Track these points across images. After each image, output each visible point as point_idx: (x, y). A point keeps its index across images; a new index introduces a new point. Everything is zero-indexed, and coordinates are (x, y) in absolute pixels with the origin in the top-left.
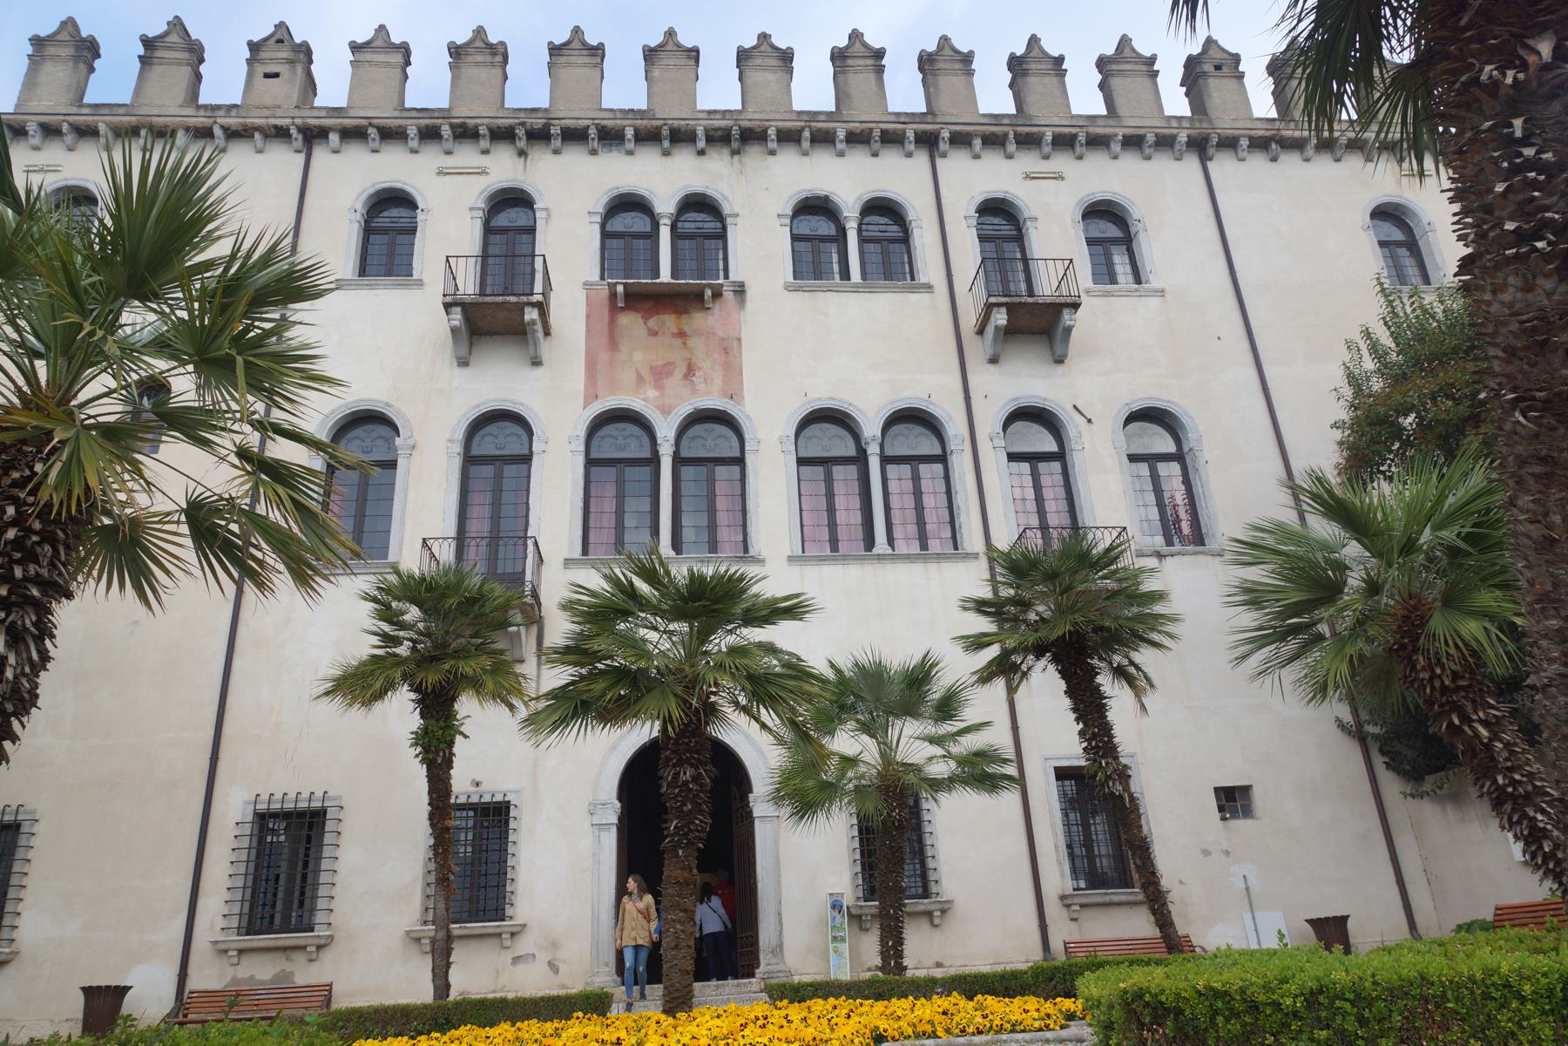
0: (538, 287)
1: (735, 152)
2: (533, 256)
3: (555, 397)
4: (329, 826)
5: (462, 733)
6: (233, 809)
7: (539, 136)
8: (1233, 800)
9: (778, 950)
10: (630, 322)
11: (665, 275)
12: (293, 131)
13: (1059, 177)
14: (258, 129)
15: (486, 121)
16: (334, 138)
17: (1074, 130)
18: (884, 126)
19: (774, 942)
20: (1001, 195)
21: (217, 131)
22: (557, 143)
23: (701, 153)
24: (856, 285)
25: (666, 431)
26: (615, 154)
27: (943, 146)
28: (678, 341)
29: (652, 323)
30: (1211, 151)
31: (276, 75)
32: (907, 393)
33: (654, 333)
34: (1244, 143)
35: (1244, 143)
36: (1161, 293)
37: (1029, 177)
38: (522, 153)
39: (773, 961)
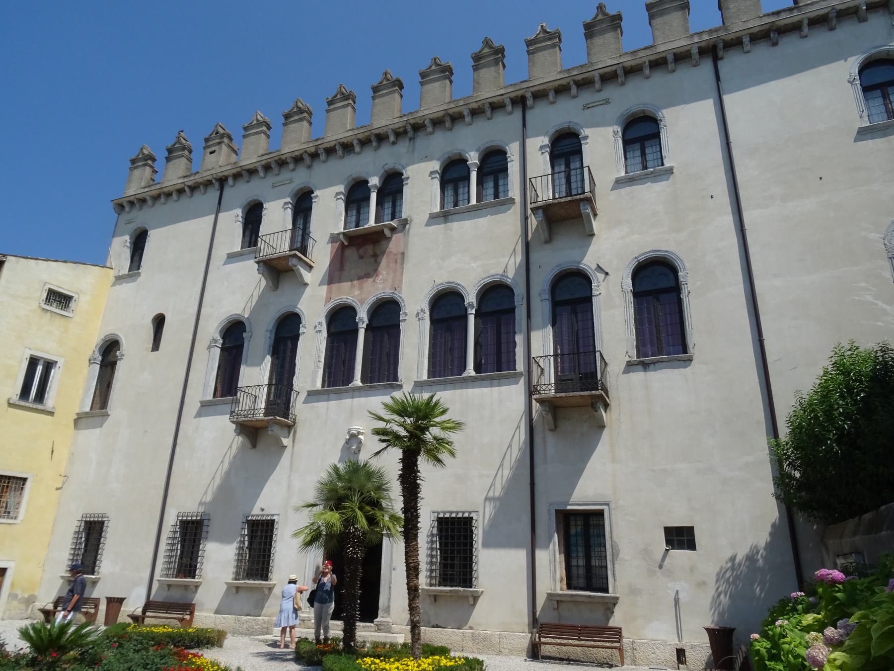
0: (587, 189)
1: (411, 139)
2: (582, 167)
3: (314, 304)
4: (204, 529)
5: (643, 154)
6: (171, 519)
7: (456, 118)
8: (680, 537)
9: (388, 610)
10: (351, 253)
11: (372, 222)
12: (214, 181)
13: (607, 102)
14: (201, 183)
15: (745, 32)
16: (230, 181)
17: (614, 68)
18: (489, 100)
19: (386, 604)
20: (566, 125)
21: (187, 189)
22: (671, 66)
23: (394, 143)
24: (476, 208)
25: (471, 298)
26: (352, 155)
27: (530, 102)
28: (372, 260)
29: (361, 251)
30: (720, 54)
31: (214, 152)
32: (492, 272)
33: (361, 257)
34: (746, 40)
35: (746, 40)
36: (670, 171)
37: (586, 107)
38: (309, 167)
39: (385, 615)
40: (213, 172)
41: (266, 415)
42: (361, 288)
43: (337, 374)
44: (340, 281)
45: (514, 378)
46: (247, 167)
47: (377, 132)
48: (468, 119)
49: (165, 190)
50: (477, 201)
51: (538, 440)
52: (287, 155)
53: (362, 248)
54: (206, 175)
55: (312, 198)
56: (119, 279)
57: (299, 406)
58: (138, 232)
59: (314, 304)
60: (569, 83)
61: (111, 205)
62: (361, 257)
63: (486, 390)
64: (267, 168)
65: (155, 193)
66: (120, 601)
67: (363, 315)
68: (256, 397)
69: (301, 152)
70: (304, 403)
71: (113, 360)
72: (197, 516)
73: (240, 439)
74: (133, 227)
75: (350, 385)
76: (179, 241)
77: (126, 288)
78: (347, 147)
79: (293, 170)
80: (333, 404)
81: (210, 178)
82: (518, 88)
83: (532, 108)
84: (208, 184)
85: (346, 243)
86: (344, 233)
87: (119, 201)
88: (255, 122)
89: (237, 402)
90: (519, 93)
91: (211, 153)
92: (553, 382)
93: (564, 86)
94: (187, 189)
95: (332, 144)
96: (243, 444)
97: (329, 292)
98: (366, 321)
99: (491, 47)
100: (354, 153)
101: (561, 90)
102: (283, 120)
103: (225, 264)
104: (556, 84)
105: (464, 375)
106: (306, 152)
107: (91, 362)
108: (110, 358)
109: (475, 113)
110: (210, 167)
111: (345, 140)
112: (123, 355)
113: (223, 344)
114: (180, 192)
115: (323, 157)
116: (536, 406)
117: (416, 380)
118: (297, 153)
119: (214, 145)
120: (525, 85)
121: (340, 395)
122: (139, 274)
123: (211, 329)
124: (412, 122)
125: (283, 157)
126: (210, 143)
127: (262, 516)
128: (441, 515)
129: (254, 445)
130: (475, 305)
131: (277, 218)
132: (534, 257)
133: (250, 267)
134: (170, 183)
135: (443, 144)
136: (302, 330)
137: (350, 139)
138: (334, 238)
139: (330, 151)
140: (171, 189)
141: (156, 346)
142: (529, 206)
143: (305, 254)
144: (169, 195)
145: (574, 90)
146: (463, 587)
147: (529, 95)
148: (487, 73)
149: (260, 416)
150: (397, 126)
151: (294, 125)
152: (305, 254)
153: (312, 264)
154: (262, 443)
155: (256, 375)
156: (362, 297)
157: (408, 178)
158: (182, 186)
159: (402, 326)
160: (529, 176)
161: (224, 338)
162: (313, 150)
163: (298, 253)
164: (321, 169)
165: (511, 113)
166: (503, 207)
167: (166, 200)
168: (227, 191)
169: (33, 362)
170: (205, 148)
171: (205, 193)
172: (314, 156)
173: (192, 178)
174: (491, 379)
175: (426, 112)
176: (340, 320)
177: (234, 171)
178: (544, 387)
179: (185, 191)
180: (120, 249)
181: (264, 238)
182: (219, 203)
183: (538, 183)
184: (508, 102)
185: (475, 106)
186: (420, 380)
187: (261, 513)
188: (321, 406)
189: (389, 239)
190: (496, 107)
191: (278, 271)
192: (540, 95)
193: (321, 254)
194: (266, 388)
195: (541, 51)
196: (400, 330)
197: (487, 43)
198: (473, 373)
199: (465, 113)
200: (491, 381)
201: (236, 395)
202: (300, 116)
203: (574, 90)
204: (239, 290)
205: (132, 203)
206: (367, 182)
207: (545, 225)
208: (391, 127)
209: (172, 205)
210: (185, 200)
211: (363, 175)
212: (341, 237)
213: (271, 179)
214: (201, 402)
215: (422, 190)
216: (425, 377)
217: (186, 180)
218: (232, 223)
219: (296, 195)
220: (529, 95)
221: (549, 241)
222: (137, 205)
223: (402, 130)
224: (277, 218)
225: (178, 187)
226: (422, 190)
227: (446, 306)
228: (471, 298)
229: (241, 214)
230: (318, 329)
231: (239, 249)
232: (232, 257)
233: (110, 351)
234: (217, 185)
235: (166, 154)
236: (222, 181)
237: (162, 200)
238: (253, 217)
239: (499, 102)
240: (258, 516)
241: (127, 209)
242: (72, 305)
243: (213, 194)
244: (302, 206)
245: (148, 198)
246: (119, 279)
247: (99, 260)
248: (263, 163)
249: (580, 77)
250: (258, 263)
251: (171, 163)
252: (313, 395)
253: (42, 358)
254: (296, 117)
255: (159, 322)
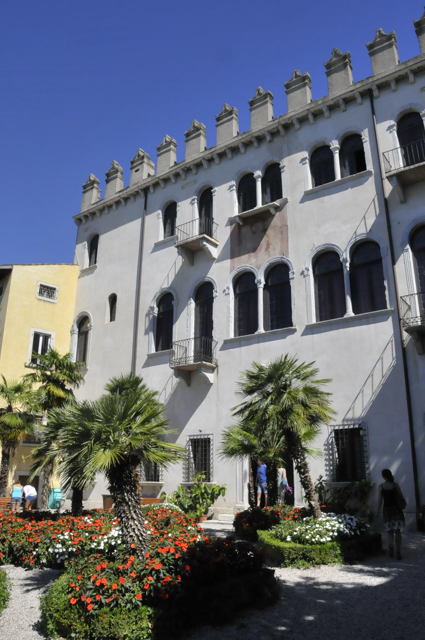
3: (222, 275)
10: (246, 230)
16: (151, 190)
21: (122, 200)
25: (345, 255)
27: (376, 93)
29: (253, 228)
40: (139, 185)
41: (195, 361)
42: (256, 257)
43: (246, 324)
44: (239, 255)
45: (383, 318)
46: (162, 178)
47: (256, 135)
48: (327, 114)
49: (108, 203)
50: (342, 177)
51: (410, 364)
52: (190, 164)
53: (252, 227)
54: (133, 188)
55: (212, 193)
56: (84, 273)
57: (217, 353)
58: (93, 237)
59: (222, 275)
60: (407, 73)
61: (73, 220)
62: (254, 233)
63: (364, 327)
64: (177, 175)
65: (101, 207)
66: (286, 92)
67: (261, 278)
68: (186, 348)
69: (201, 159)
70: (220, 350)
71: (85, 330)
72: (354, 425)
73: (176, 380)
74: (88, 234)
75: (256, 333)
76: (119, 241)
77: (88, 278)
78: (234, 150)
79: (196, 173)
80: (244, 349)
81: (137, 189)
82: (365, 83)
83: (378, 97)
84: (136, 194)
85: (241, 224)
86: (239, 216)
87: (78, 217)
88: (164, 144)
89: (173, 353)
90: (366, 87)
91: (136, 171)
92: (419, 315)
93: (403, 75)
94: (122, 200)
95: (223, 150)
96: (179, 384)
97: (232, 263)
98: (263, 282)
99: (339, 56)
100: (241, 154)
101: (401, 79)
102: (185, 138)
103: (152, 252)
104: (396, 75)
105: (345, 316)
106: (204, 159)
107: (72, 333)
108: (84, 329)
109: (332, 108)
110: (136, 182)
111: (233, 145)
112: (91, 326)
113: (158, 311)
114: (118, 203)
115: (217, 160)
116: (405, 335)
117: (307, 324)
118: (198, 161)
119: (137, 165)
120: (370, 80)
121: (249, 342)
122: (96, 267)
123: (149, 302)
124: (283, 123)
125: (188, 166)
126: (135, 164)
127: (201, 435)
128: (337, 428)
129: (189, 384)
130: (349, 259)
131: (188, 212)
132: (393, 216)
133: (172, 251)
134: (110, 198)
135: (311, 135)
136: (214, 294)
137: (236, 144)
138: (231, 221)
139: (222, 155)
140: (111, 202)
141: (112, 318)
142: (384, 176)
143: (211, 236)
144: (110, 207)
145: (411, 77)
146: (342, 481)
147: (374, 88)
148: (337, 77)
149: (192, 362)
150: (271, 128)
151: (193, 141)
152: (211, 236)
153: (217, 243)
154: (195, 381)
155: (185, 326)
156: (258, 263)
157: (284, 167)
158: (119, 198)
159: (292, 283)
160: (381, 151)
161: (158, 306)
162: (210, 156)
163: (205, 236)
164: (217, 168)
165: (361, 104)
166: (364, 178)
167: (109, 211)
168: (150, 197)
169: (37, 336)
170: (131, 169)
171: (135, 201)
172: (210, 160)
173: (125, 192)
174: (367, 317)
175: (293, 114)
176: (244, 283)
177: (154, 182)
178: (412, 320)
179: (121, 202)
180: (82, 250)
181: (180, 228)
182: (145, 208)
183: (390, 156)
184: (358, 96)
185: (332, 103)
186: (310, 324)
187: (199, 433)
188: (235, 351)
189: (273, 216)
190: (348, 101)
191: (192, 252)
192: (383, 86)
193: (222, 233)
194: (193, 341)
195: (380, 52)
196: (290, 286)
197: (336, 54)
198: (353, 315)
199: (324, 110)
200: (368, 321)
201: (172, 348)
202: (197, 133)
203: (411, 77)
204: (164, 269)
205: (86, 217)
206: (253, 174)
207: (399, 190)
208: (266, 129)
209: (115, 213)
210: (122, 209)
211: (249, 170)
212: (237, 219)
213: (181, 183)
214: (148, 355)
215: (297, 173)
216: (314, 321)
217: (121, 194)
218: (155, 221)
219: (200, 192)
220: (374, 88)
221: (404, 201)
222: (90, 218)
223: (275, 130)
224: (188, 212)
225: (115, 200)
226: (297, 173)
227: (325, 262)
228: (345, 255)
229: (161, 214)
230: (227, 292)
231: (163, 239)
232: (158, 246)
233: (83, 325)
234: (142, 194)
235: (106, 178)
236: (146, 190)
237: (106, 211)
238: (170, 214)
239: (350, 97)
240: (198, 435)
241: (84, 221)
242: (56, 294)
243: (141, 201)
244: (205, 201)
245: (97, 211)
246: (84, 273)
247: (69, 260)
248: (174, 172)
249: (415, 67)
250: (177, 247)
251: (109, 185)
252: (228, 344)
253: (42, 333)
254: (194, 135)
255: (113, 299)
